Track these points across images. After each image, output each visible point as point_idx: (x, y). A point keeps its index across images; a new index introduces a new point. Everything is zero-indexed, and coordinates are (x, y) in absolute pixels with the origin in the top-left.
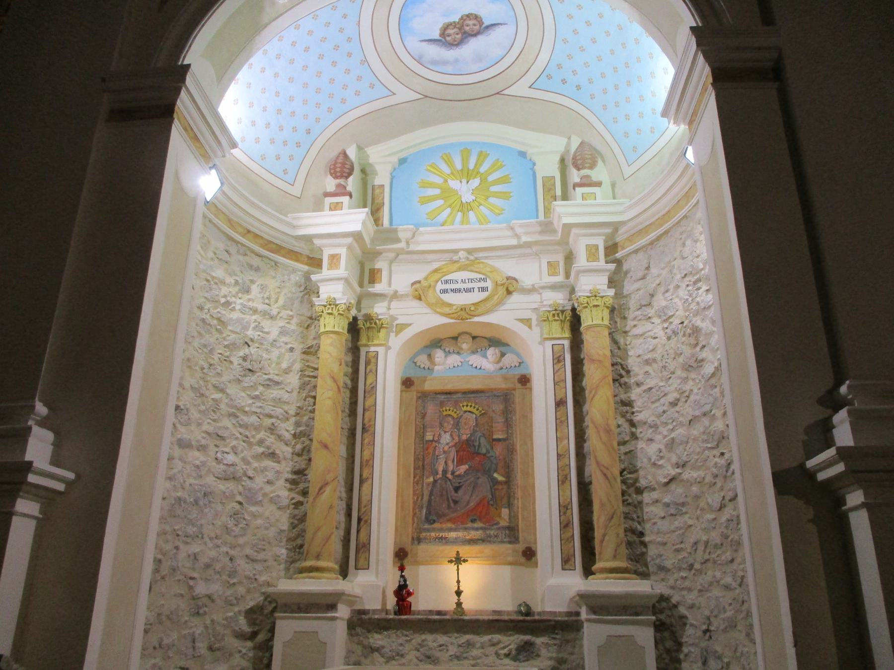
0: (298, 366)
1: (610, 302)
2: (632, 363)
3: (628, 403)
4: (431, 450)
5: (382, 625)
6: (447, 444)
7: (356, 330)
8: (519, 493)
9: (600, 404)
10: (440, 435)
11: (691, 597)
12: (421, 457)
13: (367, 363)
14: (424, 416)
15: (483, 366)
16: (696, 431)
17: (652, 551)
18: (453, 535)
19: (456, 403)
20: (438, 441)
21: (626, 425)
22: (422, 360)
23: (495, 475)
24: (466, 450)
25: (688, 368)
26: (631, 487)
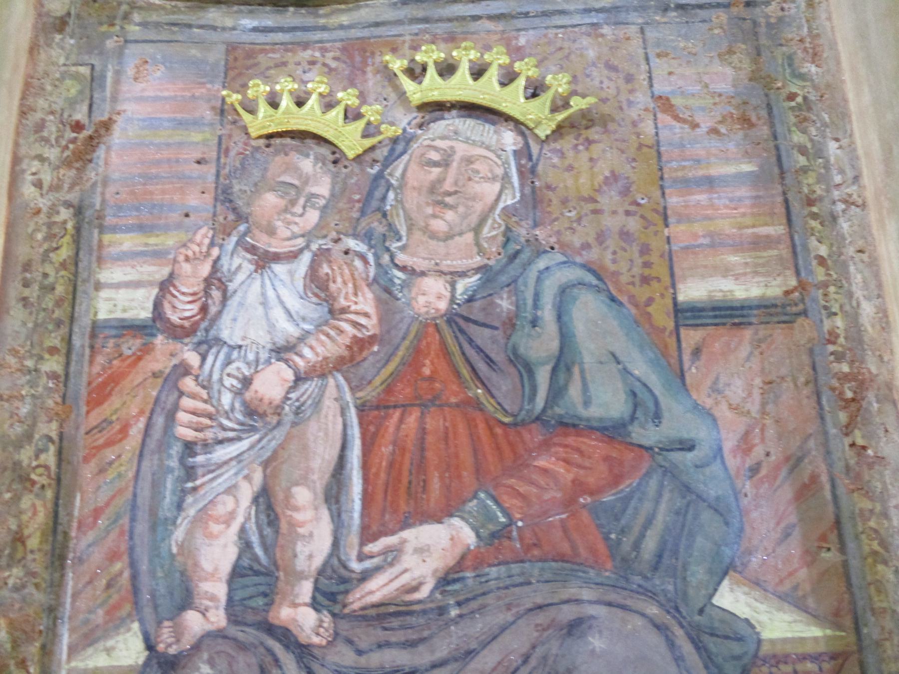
4: (130, 404)
6: (282, 351)
10: (216, 281)
20: (200, 331)
23: (732, 599)
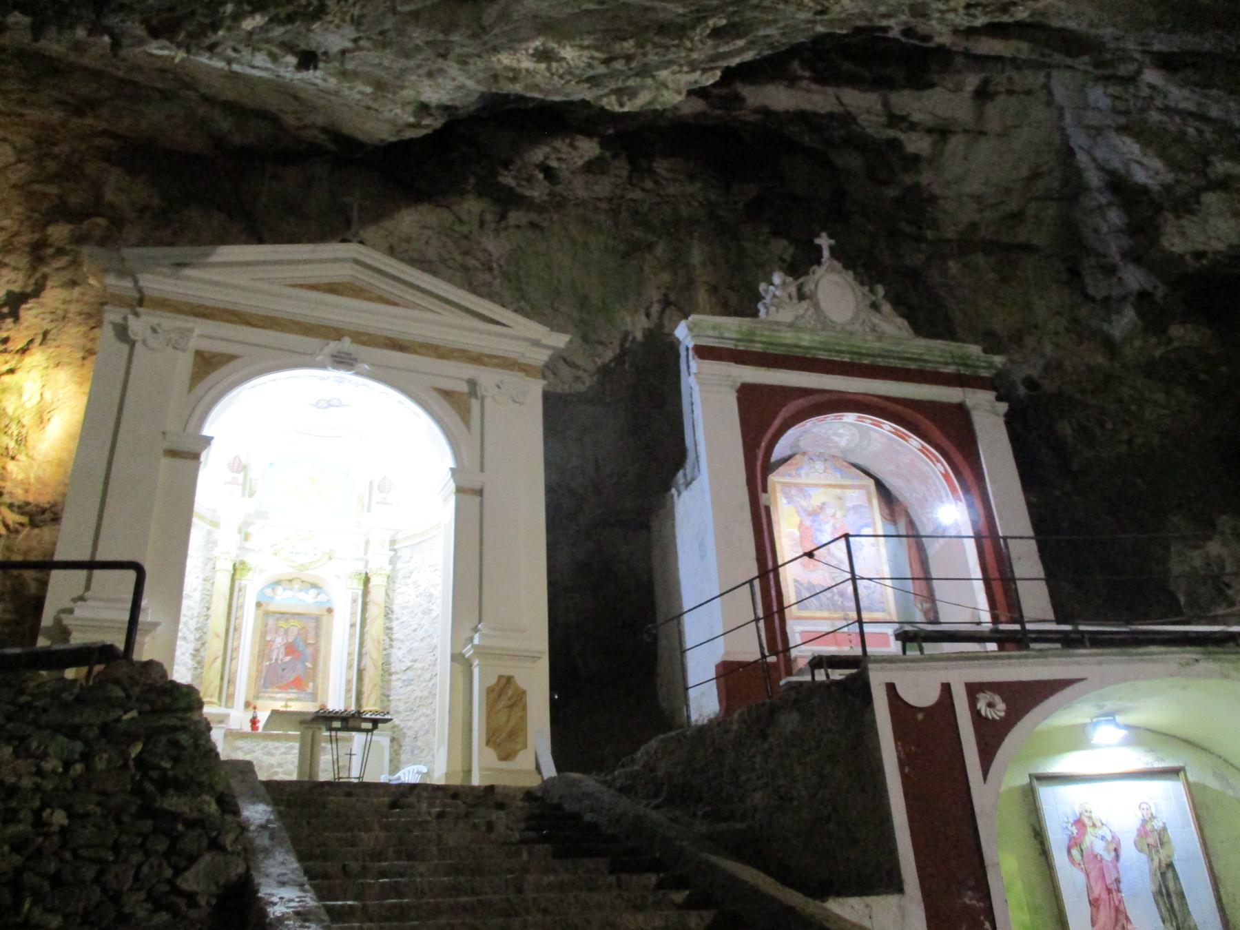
0: (200, 588)
1: (388, 573)
2: (395, 607)
3: (390, 629)
5: (243, 735)
7: (237, 570)
8: (320, 675)
9: (375, 627)
11: (410, 724)
12: (264, 649)
13: (240, 590)
14: (266, 625)
15: (305, 601)
16: (423, 645)
17: (393, 704)
18: (279, 695)
19: (287, 620)
21: (388, 641)
22: (268, 592)
24: (290, 649)
25: (424, 613)
26: (386, 671)
